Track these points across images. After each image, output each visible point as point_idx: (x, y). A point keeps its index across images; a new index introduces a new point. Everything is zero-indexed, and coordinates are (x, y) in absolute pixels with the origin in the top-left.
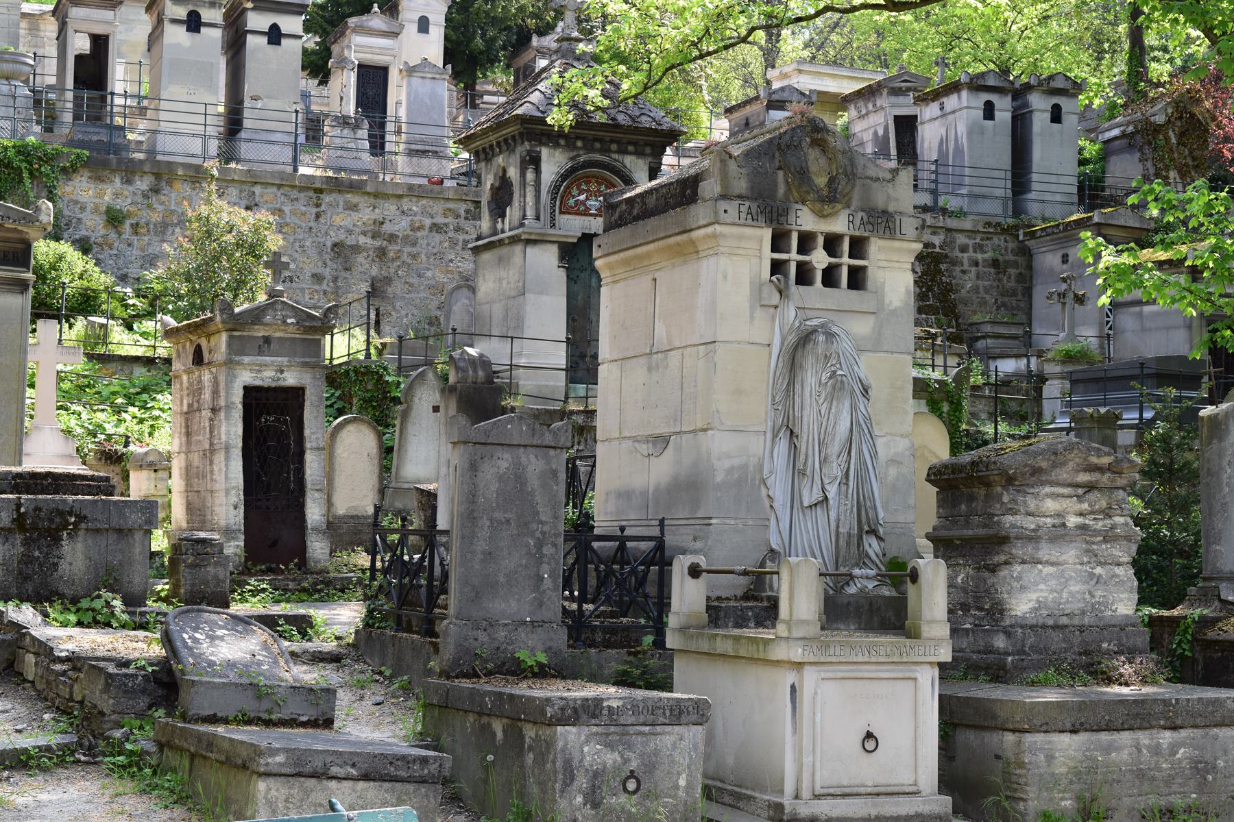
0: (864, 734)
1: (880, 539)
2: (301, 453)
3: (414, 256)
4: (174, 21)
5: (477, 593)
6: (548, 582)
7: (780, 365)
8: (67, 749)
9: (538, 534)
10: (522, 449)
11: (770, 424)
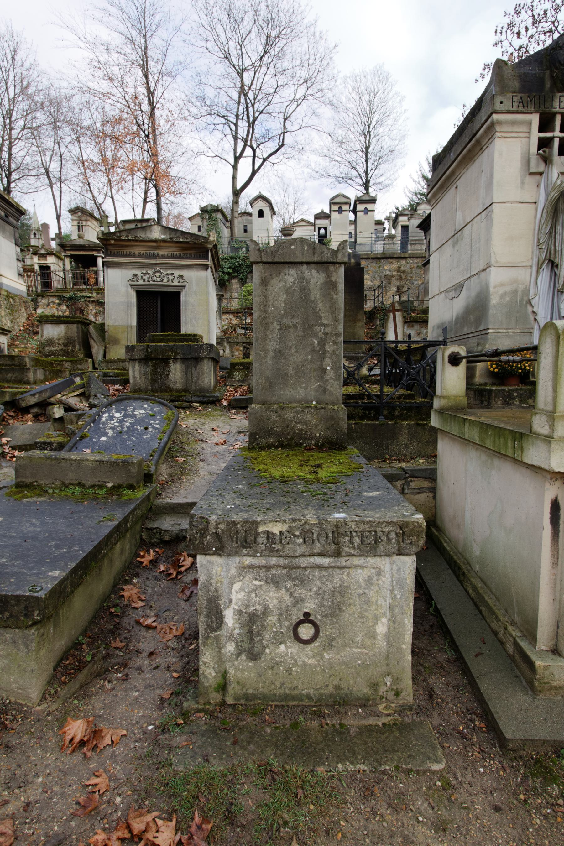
3: (411, 277)
5: (271, 383)
7: (545, 215)
9: (321, 335)
10: (305, 266)
11: (535, 260)
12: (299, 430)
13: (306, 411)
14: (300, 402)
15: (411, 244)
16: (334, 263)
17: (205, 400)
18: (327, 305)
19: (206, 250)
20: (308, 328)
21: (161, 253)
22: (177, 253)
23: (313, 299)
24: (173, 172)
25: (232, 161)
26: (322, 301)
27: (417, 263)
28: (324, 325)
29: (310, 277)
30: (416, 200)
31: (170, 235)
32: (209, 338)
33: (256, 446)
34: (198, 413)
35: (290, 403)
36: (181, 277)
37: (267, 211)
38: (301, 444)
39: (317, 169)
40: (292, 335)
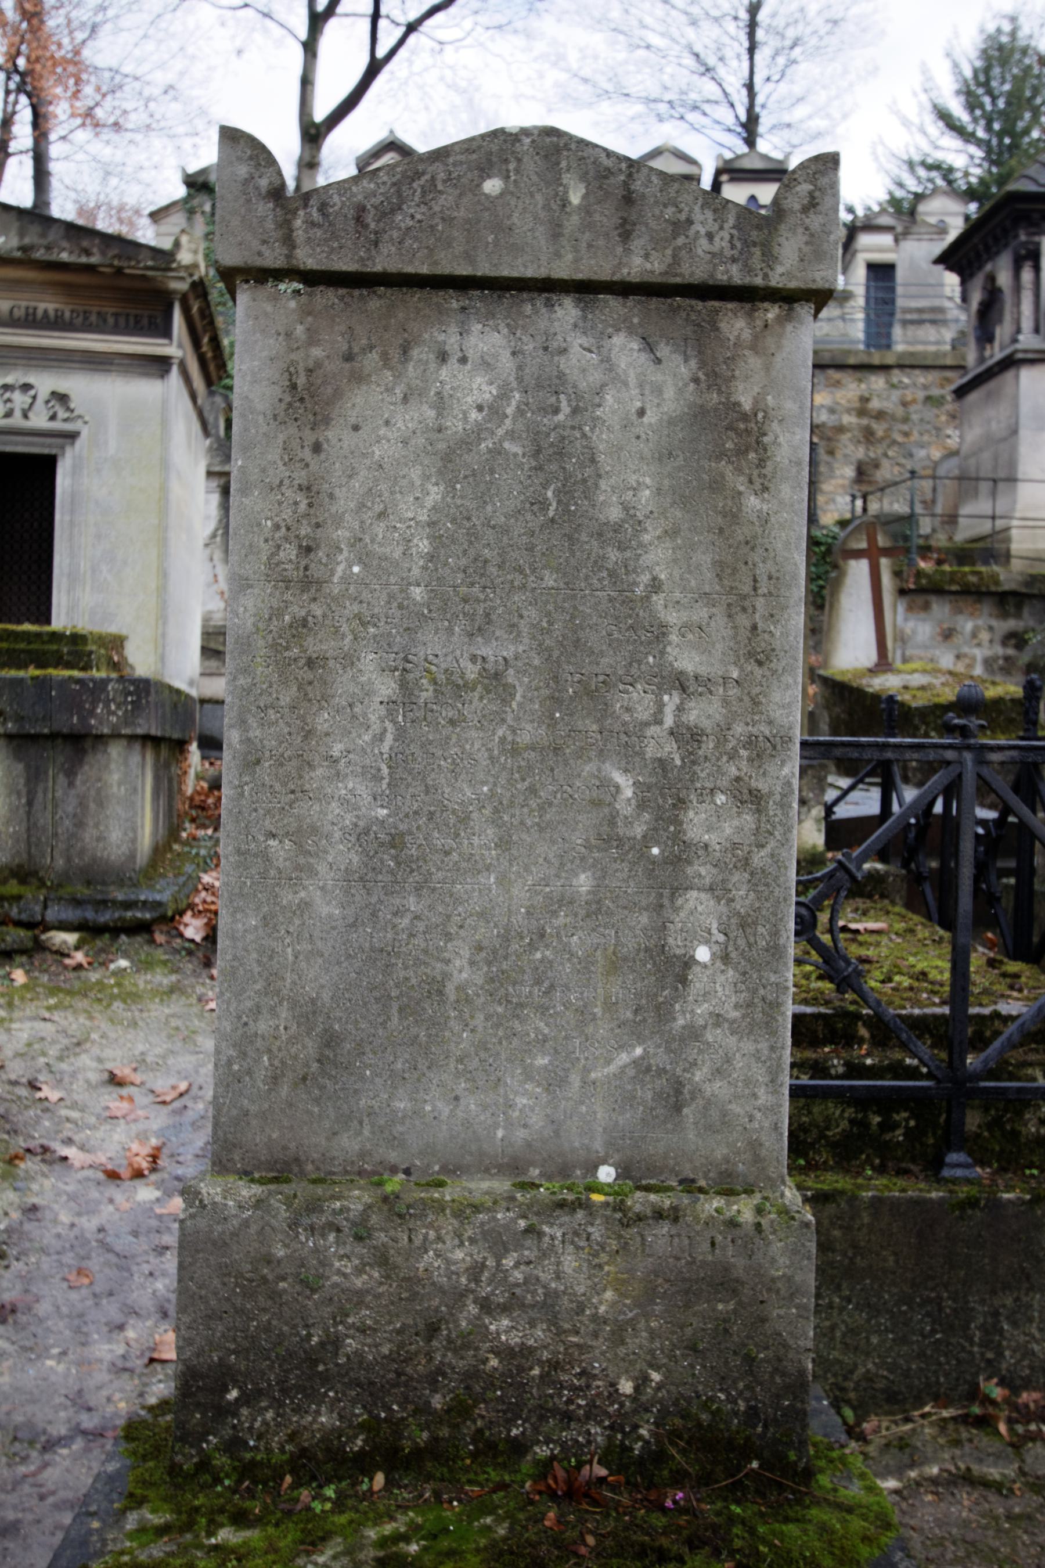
3: (906, 434)
5: (330, 1040)
6: (713, 986)
9: (659, 744)
10: (567, 311)
12: (506, 1353)
13: (552, 1231)
14: (513, 1166)
15: (905, 323)
16: (747, 296)
17: (105, 917)
18: (704, 559)
19: (163, 300)
20: (579, 697)
22: (48, 305)
23: (615, 514)
24: (100, 54)
26: (672, 533)
27: (925, 387)
28: (680, 683)
29: (596, 377)
30: (913, 185)
31: (21, 235)
32: (161, 644)
33: (221, 1460)
34: (70, 989)
35: (454, 1170)
36: (62, 398)
38: (519, 1448)
39: (586, 72)
40: (475, 741)
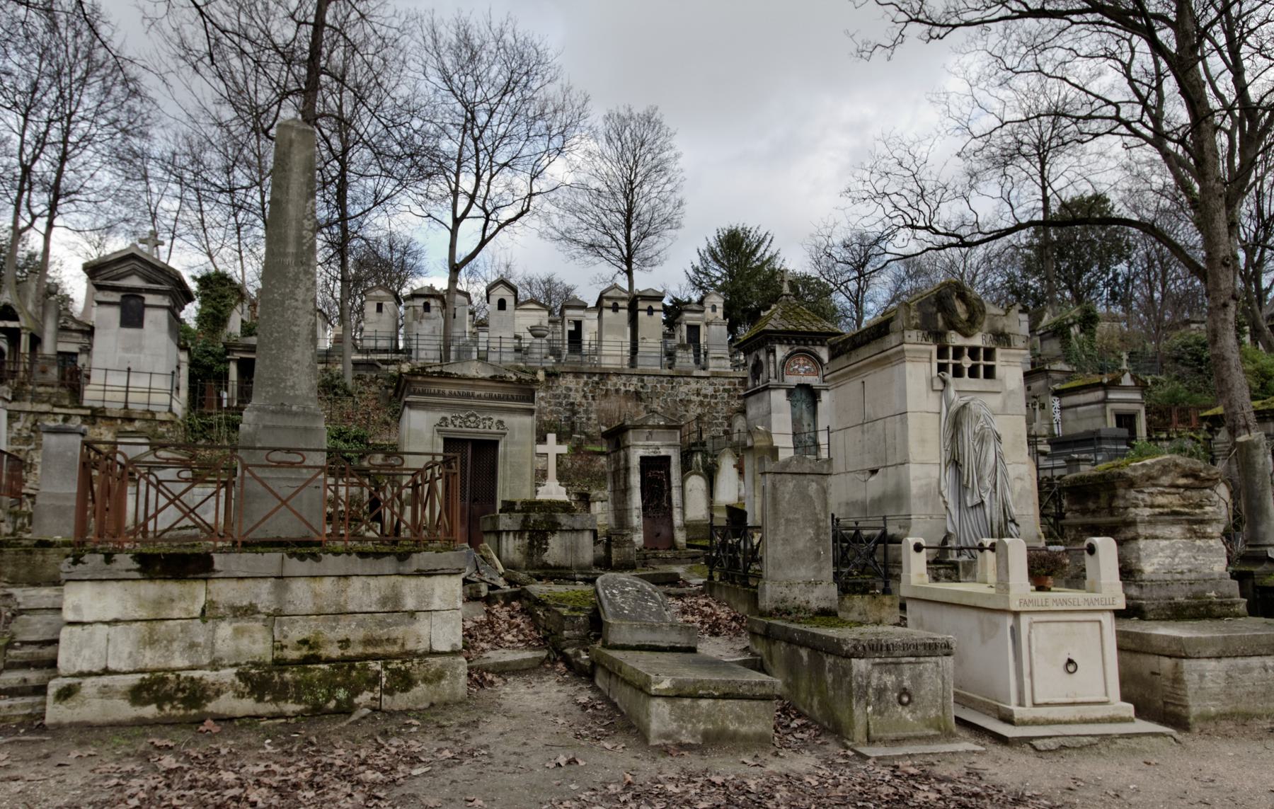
0: (1065, 661)
1: (1017, 525)
2: (670, 489)
4: (608, 308)
8: (542, 662)
21: (477, 393)
25: (449, 222)
37: (510, 302)
